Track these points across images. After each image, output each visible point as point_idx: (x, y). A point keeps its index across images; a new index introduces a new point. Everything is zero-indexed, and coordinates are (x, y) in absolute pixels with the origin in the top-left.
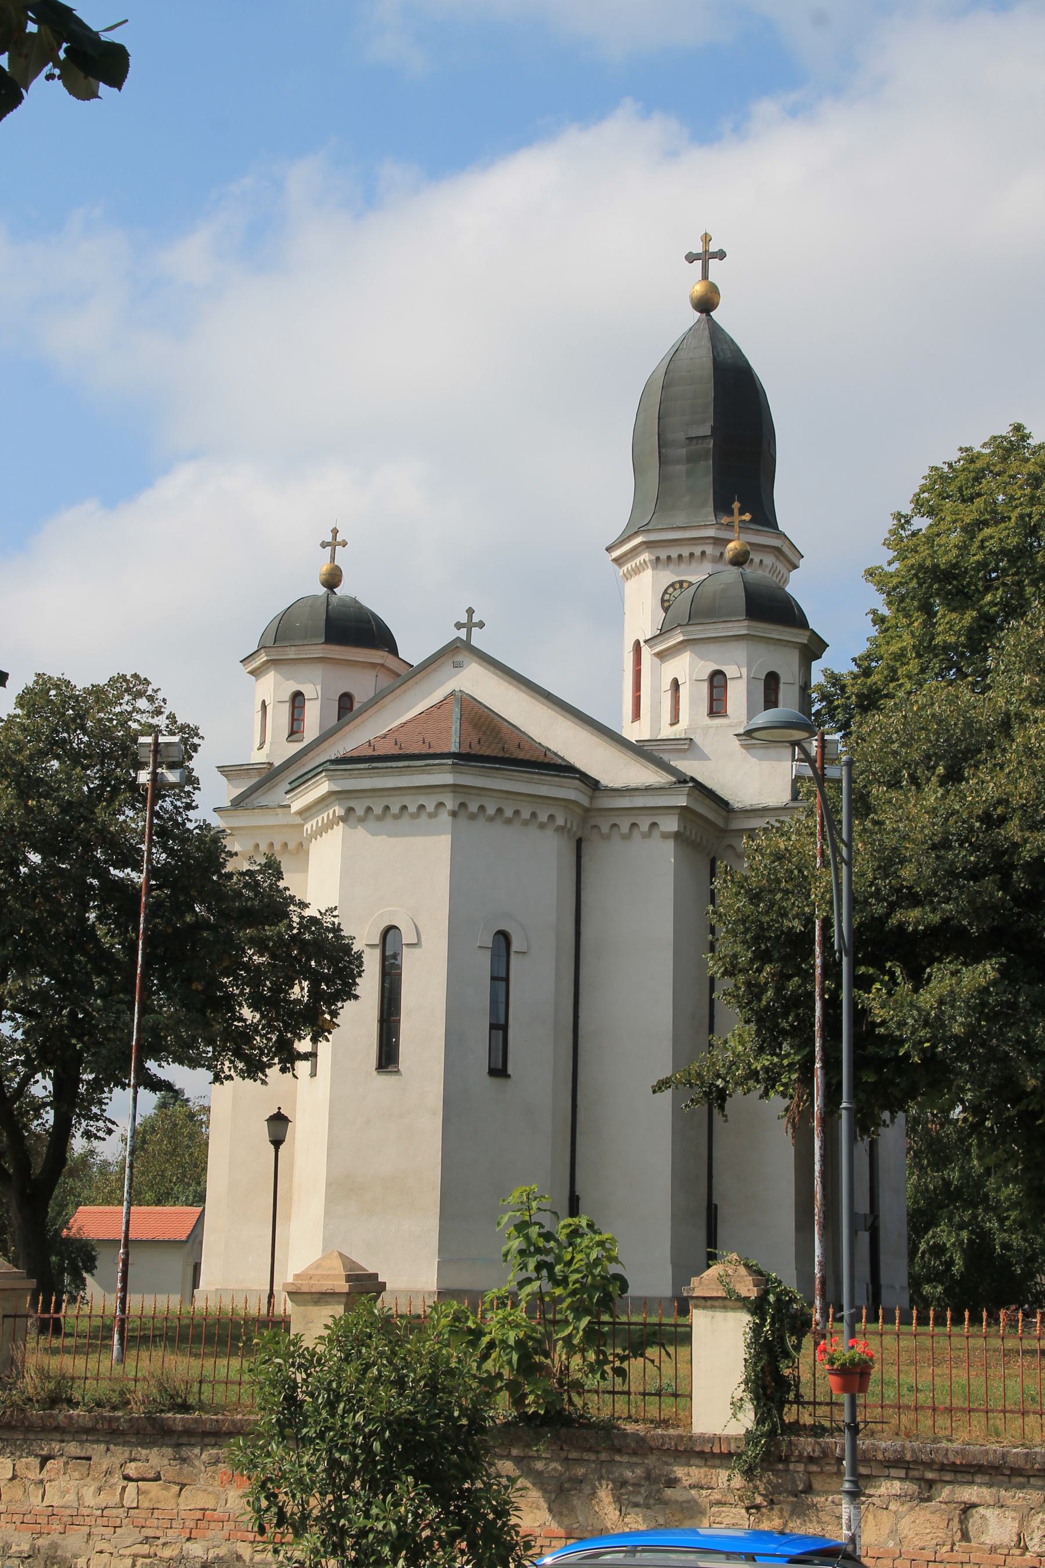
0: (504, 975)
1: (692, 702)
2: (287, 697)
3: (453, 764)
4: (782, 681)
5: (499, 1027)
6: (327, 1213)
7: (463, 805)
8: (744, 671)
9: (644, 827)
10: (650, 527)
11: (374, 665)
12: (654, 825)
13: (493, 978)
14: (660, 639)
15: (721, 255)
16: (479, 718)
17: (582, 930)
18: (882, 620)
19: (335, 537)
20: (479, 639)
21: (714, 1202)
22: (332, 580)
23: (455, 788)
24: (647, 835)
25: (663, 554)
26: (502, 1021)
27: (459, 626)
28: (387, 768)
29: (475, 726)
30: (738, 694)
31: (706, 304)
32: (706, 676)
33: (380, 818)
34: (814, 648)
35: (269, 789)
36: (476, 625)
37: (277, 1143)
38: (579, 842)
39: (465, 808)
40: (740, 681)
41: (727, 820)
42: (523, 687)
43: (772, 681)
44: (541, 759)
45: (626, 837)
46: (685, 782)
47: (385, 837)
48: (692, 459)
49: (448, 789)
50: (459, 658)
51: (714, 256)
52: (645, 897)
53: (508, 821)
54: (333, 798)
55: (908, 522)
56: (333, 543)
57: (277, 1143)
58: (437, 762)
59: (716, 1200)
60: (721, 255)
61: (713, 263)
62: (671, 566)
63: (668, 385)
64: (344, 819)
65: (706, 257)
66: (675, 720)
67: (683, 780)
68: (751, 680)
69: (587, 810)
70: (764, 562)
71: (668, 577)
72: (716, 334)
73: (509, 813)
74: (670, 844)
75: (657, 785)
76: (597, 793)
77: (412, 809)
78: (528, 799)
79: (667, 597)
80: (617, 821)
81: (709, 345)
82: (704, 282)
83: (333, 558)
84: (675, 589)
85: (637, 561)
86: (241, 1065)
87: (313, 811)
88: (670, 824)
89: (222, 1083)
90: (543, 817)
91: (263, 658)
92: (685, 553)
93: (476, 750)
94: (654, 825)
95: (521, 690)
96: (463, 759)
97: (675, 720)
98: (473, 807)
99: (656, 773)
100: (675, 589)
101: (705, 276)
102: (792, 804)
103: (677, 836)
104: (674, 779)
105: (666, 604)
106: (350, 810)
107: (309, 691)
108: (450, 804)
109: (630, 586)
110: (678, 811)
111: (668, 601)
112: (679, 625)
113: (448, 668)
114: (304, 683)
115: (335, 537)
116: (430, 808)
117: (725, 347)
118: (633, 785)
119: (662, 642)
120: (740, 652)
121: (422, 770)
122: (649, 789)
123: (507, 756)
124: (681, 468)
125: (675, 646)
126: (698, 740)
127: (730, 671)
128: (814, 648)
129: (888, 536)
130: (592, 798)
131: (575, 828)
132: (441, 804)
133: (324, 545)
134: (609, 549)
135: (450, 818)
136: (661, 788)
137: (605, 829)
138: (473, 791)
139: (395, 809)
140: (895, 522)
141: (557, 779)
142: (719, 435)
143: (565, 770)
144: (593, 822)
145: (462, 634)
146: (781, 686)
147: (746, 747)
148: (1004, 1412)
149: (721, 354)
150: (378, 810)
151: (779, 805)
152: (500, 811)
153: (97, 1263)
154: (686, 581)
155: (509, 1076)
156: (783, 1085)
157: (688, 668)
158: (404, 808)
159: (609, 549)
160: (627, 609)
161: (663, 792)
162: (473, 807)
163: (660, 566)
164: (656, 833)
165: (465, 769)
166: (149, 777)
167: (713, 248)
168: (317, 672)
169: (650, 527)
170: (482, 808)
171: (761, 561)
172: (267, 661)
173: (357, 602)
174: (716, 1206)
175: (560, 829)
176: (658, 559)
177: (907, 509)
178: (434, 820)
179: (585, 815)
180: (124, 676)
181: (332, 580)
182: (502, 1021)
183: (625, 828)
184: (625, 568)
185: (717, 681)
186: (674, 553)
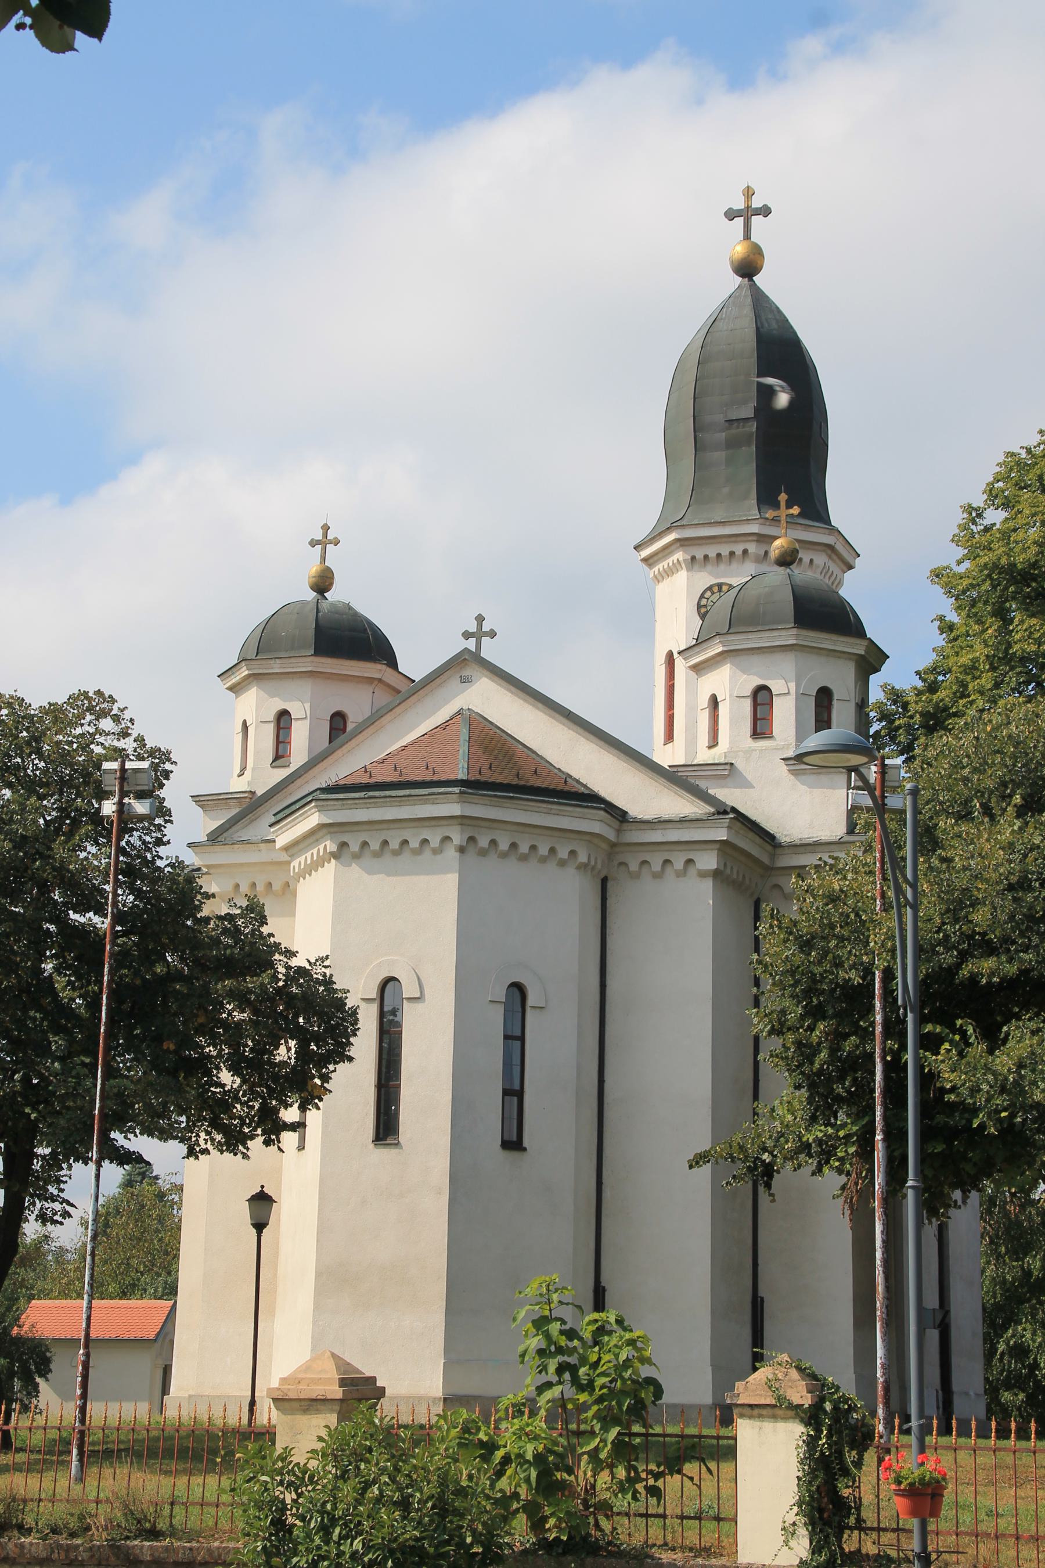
0: (518, 1033)
1: (733, 722)
2: (271, 716)
3: (461, 793)
4: (836, 697)
5: (514, 1094)
6: (317, 1307)
7: (472, 839)
8: (792, 686)
9: (679, 864)
11: (370, 680)
13: (507, 1037)
14: (697, 649)
15: (765, 211)
16: (489, 740)
19: (325, 535)
20: (489, 650)
21: (761, 1294)
22: (323, 584)
23: (463, 820)
24: (682, 874)
26: (517, 1087)
27: (467, 635)
29: (486, 749)
30: (785, 714)
32: (748, 691)
33: (377, 855)
34: (872, 660)
35: (252, 821)
36: (486, 634)
37: (260, 1227)
38: (604, 881)
39: (475, 842)
40: (788, 697)
41: (773, 857)
42: (540, 705)
43: (824, 697)
45: (658, 876)
46: (725, 812)
48: (732, 444)
49: (455, 821)
50: (466, 672)
51: (758, 212)
52: (681, 948)
53: (524, 858)
55: (980, 516)
56: (324, 541)
57: (260, 1227)
58: (442, 790)
60: (765, 211)
62: (709, 567)
63: (705, 361)
65: (748, 213)
66: (713, 743)
67: (723, 810)
68: (800, 696)
69: (613, 845)
70: (815, 562)
71: (705, 579)
72: (760, 302)
73: (524, 848)
74: (708, 884)
77: (414, 844)
79: (704, 602)
82: (746, 243)
83: (323, 559)
84: (713, 593)
85: (665, 564)
86: (219, 1137)
87: (301, 846)
88: (709, 861)
89: (197, 1158)
90: (563, 853)
91: (244, 672)
93: (487, 777)
95: (538, 708)
96: (472, 786)
97: (713, 743)
98: (483, 842)
99: (692, 803)
100: (713, 593)
101: (747, 236)
102: (847, 838)
103: (716, 874)
104: (712, 810)
106: (343, 845)
107: (296, 709)
108: (458, 837)
109: (662, 589)
110: (717, 846)
111: (705, 606)
112: (718, 634)
113: (454, 683)
115: (325, 535)
116: (435, 842)
118: (666, 817)
119: (698, 653)
120: (788, 663)
121: (423, 800)
123: (522, 783)
126: (740, 764)
127: (776, 686)
129: (957, 531)
130: (618, 831)
131: (599, 866)
132: (447, 839)
135: (457, 854)
137: (634, 866)
139: (394, 844)
140: (965, 515)
141: (578, 809)
142: (763, 422)
143: (589, 799)
144: (621, 858)
146: (835, 702)
147: (794, 773)
150: (375, 845)
152: (514, 846)
153: (52, 1366)
155: (525, 1149)
157: (728, 683)
158: (405, 842)
159: (637, 548)
161: (700, 824)
162: (483, 842)
163: (696, 567)
164: (692, 871)
167: (756, 203)
168: (306, 687)
170: (493, 842)
171: (811, 561)
172: (249, 676)
173: (350, 608)
174: (762, 1299)
175: (583, 867)
176: (693, 558)
177: (979, 500)
178: (438, 857)
179: (611, 851)
181: (323, 584)
182: (517, 1087)
183: (657, 866)
184: (656, 569)
186: (712, 551)
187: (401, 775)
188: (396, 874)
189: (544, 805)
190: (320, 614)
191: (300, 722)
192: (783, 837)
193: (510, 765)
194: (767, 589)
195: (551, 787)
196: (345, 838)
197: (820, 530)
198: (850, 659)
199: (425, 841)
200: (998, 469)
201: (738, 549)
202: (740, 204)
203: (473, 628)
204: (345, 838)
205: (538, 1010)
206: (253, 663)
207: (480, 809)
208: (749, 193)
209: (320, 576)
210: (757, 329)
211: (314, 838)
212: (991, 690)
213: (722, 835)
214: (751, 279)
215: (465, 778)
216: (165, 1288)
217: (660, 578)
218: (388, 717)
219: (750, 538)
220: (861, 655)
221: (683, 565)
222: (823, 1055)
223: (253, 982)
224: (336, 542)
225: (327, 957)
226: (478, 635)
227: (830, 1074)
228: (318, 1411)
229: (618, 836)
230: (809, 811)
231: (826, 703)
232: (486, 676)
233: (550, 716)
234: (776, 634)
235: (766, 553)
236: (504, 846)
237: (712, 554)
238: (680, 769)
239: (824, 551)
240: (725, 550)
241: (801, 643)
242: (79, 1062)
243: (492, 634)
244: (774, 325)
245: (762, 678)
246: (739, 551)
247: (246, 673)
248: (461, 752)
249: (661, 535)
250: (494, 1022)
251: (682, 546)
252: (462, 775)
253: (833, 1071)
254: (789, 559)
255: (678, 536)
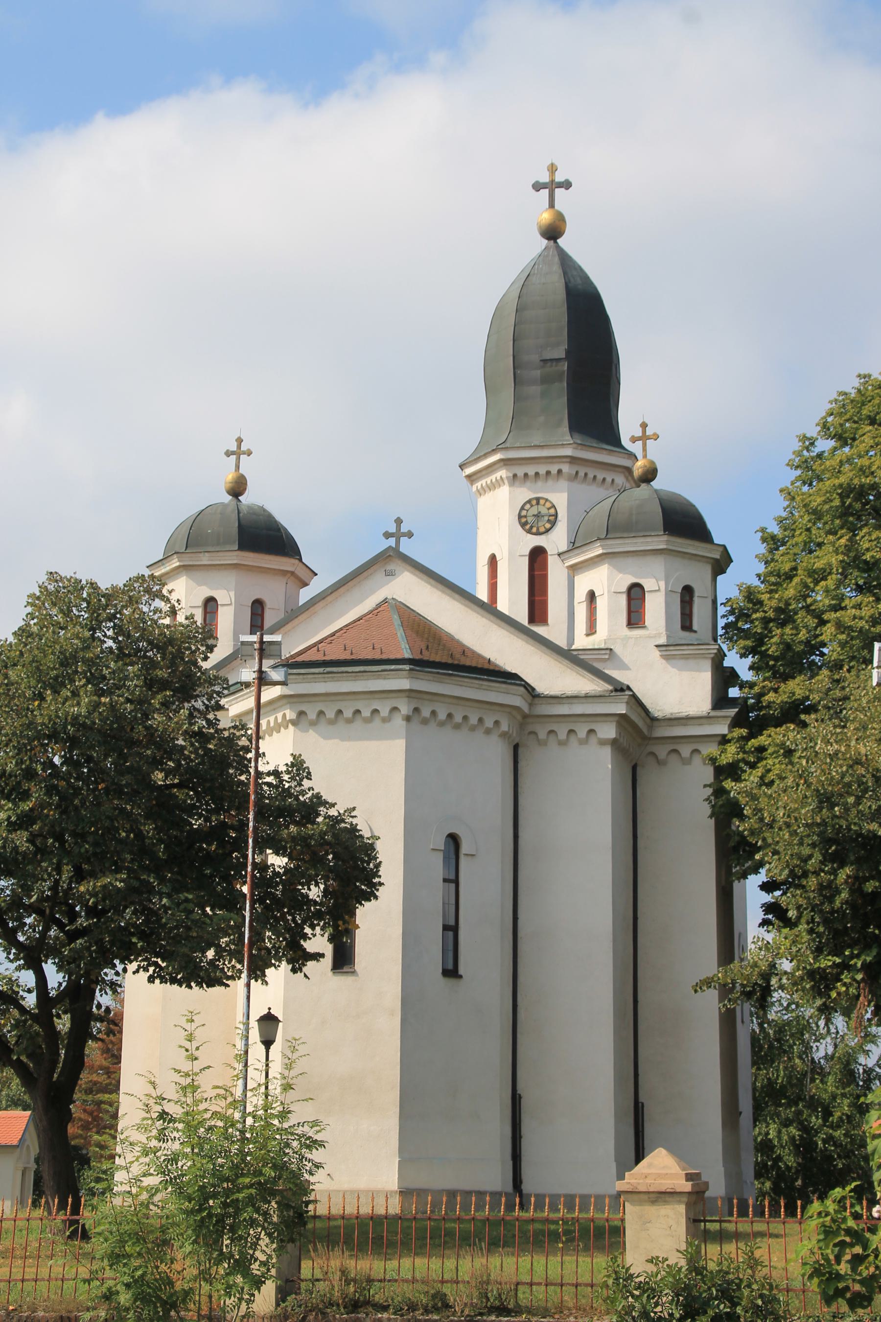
0: (452, 877)
1: (611, 614)
2: (200, 602)
3: (411, 670)
4: (696, 594)
5: (452, 929)
7: (416, 710)
8: (662, 584)
9: (582, 733)
10: (508, 445)
11: (284, 573)
12: (591, 731)
13: (445, 880)
14: (571, 554)
15: (567, 185)
16: (419, 627)
17: (521, 834)
18: (773, 537)
19: (239, 447)
20: (407, 547)
21: (641, 1099)
22: (237, 489)
23: (410, 694)
24: (584, 742)
25: (520, 471)
26: (452, 922)
27: (387, 535)
28: (342, 672)
29: (417, 633)
30: (656, 608)
31: (553, 233)
33: (332, 722)
36: (404, 535)
39: (419, 713)
40: (658, 593)
41: (651, 728)
42: (457, 596)
43: (688, 592)
44: (486, 666)
46: (622, 690)
47: (336, 741)
48: (546, 380)
49: (403, 694)
50: (391, 567)
51: (560, 185)
52: (582, 790)
53: (457, 727)
54: (285, 701)
55: (812, 444)
56: (238, 452)
58: (393, 667)
59: (642, 1099)
60: (567, 185)
61: (559, 192)
62: (528, 484)
63: (521, 307)
64: (294, 723)
65: (552, 187)
66: (591, 629)
67: (620, 689)
68: (669, 593)
69: (525, 716)
70: (616, 481)
71: (525, 494)
72: (566, 262)
73: (458, 719)
74: (607, 751)
75: (593, 693)
76: (536, 700)
77: (366, 713)
78: (487, 706)
79: (524, 513)
80: (554, 727)
81: (560, 271)
82: (551, 210)
83: (238, 467)
84: (532, 506)
85: (488, 480)
88: (609, 731)
90: (489, 723)
91: (175, 563)
92: (542, 470)
93: (426, 656)
94: (591, 731)
95: (454, 599)
96: (418, 664)
97: (591, 629)
98: (426, 713)
99: (592, 681)
100: (532, 506)
101: (552, 205)
102: (713, 713)
103: (614, 743)
104: (611, 688)
105: (523, 520)
106: (301, 714)
107: (222, 596)
108: (405, 709)
109: (483, 502)
110: (616, 718)
111: (525, 517)
112: (599, 539)
113: (379, 576)
114: (217, 589)
115: (239, 447)
116: (385, 712)
117: (575, 273)
118: (569, 693)
119: (583, 552)
120: (658, 565)
121: (377, 675)
122: (587, 697)
123: (456, 662)
124: (535, 390)
125: (592, 559)
126: (618, 649)
127: (648, 584)
128: (721, 564)
130: (531, 705)
132: (395, 709)
133: (228, 454)
134: (462, 466)
135: (404, 723)
136: (600, 696)
137: (542, 735)
138: (425, 696)
139: (348, 713)
140: (801, 444)
141: (504, 686)
142: (567, 361)
144: (530, 728)
145: (392, 542)
146: (696, 599)
147: (666, 658)
148: (592, 1286)
149: (572, 280)
150: (330, 714)
151: (699, 714)
154: (543, 498)
155: (461, 977)
156: (845, 984)
157: (605, 581)
158: (358, 712)
159: (462, 466)
160: (480, 523)
161: (603, 700)
162: (426, 713)
163: (517, 483)
164: (593, 740)
165: (421, 675)
166: (255, 675)
167: (559, 178)
168: (231, 577)
169: (508, 445)
170: (434, 713)
171: (613, 480)
172: (179, 567)
173: (265, 510)
174: (643, 1104)
175: (504, 735)
176: (515, 476)
177: (813, 431)
178: (387, 725)
179: (526, 723)
180: (143, 576)
181: (237, 489)
182: (452, 922)
183: (562, 735)
184: (479, 484)
185: (635, 595)
186: (531, 470)
187: (352, 654)
188: (349, 739)
189: (477, 682)
190: (241, 515)
191: (225, 608)
192: (656, 714)
193: (441, 647)
194: (637, 502)
195: (480, 666)
196: (303, 707)
197: (621, 455)
198: (707, 562)
199: (375, 711)
200: (830, 406)
201: (554, 469)
202: (545, 178)
203: (393, 529)
204: (303, 707)
205: (470, 858)
206: (183, 555)
207: (426, 684)
208: (553, 169)
209: (236, 482)
210: (566, 283)
211: (272, 707)
212: (834, 590)
213: (622, 709)
214: (555, 242)
215: (411, 657)
216: (7, 1101)
217: (482, 491)
218: (321, 604)
219: (564, 460)
220: (716, 560)
221: (506, 482)
222: (844, 895)
223: (312, 829)
224: (249, 453)
225: (354, 809)
226: (398, 535)
227: (844, 912)
228: (666, 1202)
229: (530, 709)
230: (679, 691)
231: (687, 598)
232: (408, 571)
233: (466, 606)
234: (649, 539)
235: (577, 473)
236: (442, 716)
237: (531, 473)
238: (580, 652)
239: (623, 473)
240: (542, 470)
241: (671, 547)
242: (183, 898)
243: (410, 535)
244: (579, 281)
245: (636, 577)
246: (554, 471)
247: (178, 564)
248: (399, 635)
249: (486, 455)
250: (437, 867)
251: (505, 465)
252: (407, 655)
253: (846, 909)
254: (650, 476)
255: (502, 457)
